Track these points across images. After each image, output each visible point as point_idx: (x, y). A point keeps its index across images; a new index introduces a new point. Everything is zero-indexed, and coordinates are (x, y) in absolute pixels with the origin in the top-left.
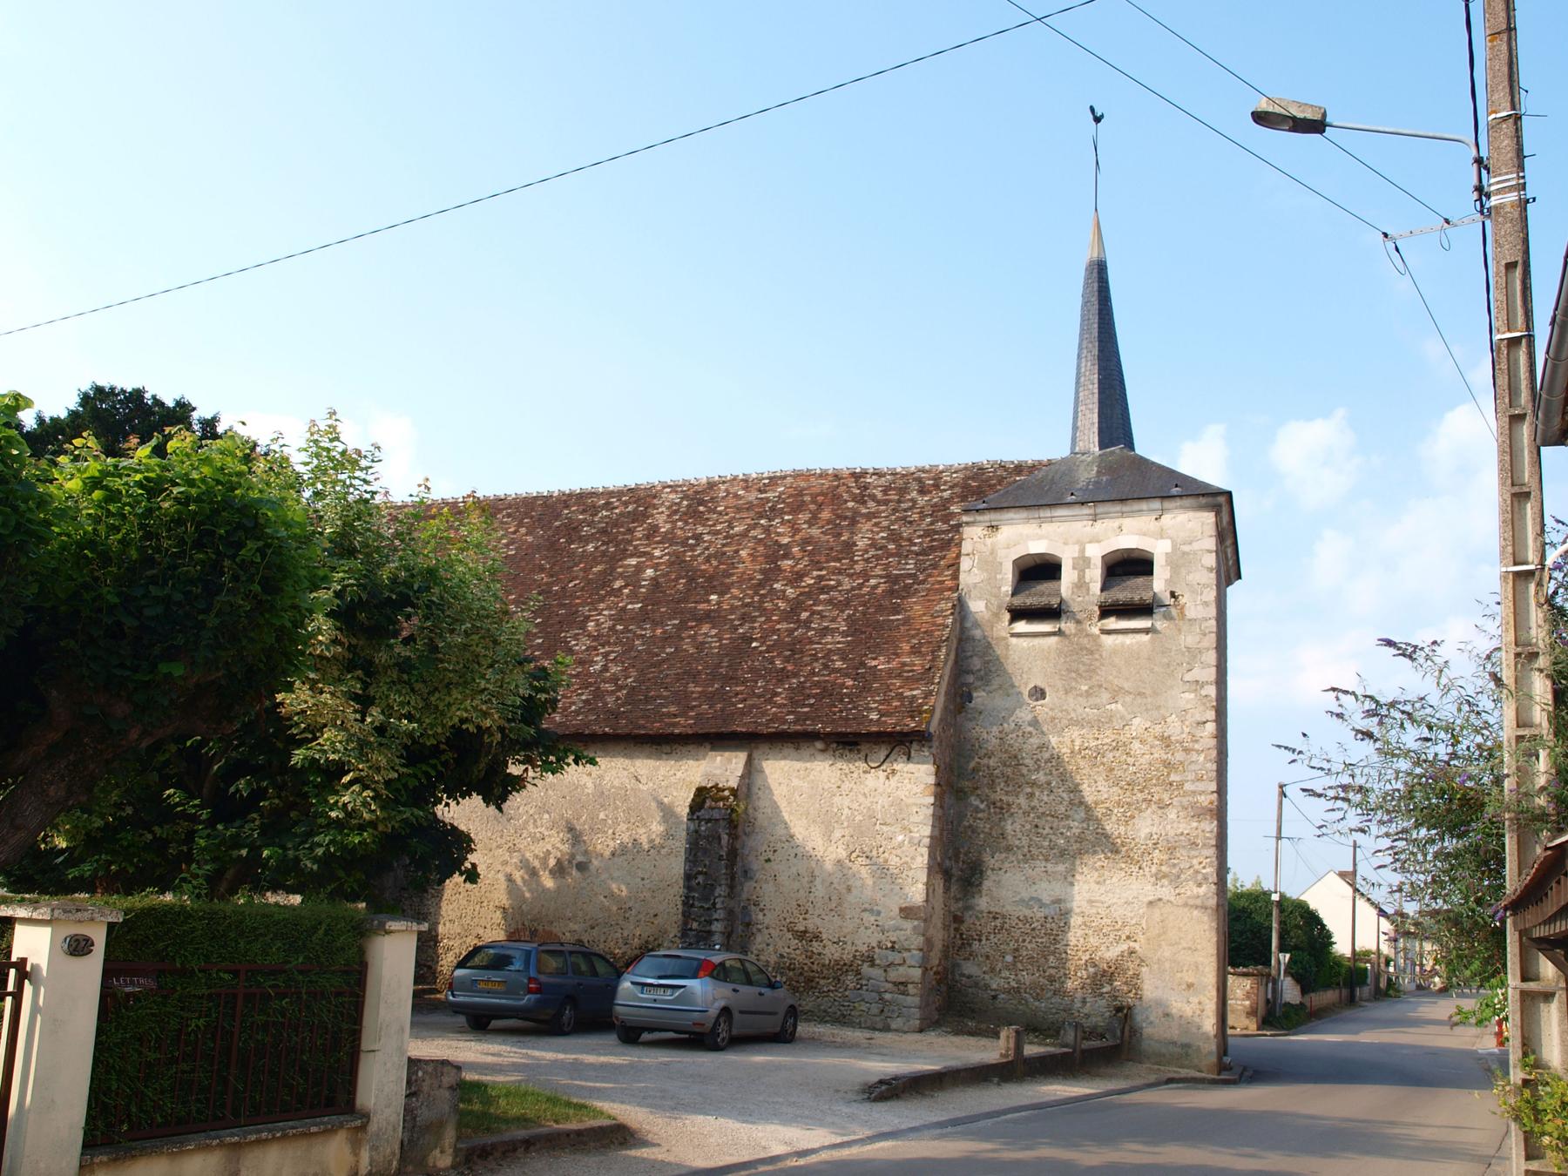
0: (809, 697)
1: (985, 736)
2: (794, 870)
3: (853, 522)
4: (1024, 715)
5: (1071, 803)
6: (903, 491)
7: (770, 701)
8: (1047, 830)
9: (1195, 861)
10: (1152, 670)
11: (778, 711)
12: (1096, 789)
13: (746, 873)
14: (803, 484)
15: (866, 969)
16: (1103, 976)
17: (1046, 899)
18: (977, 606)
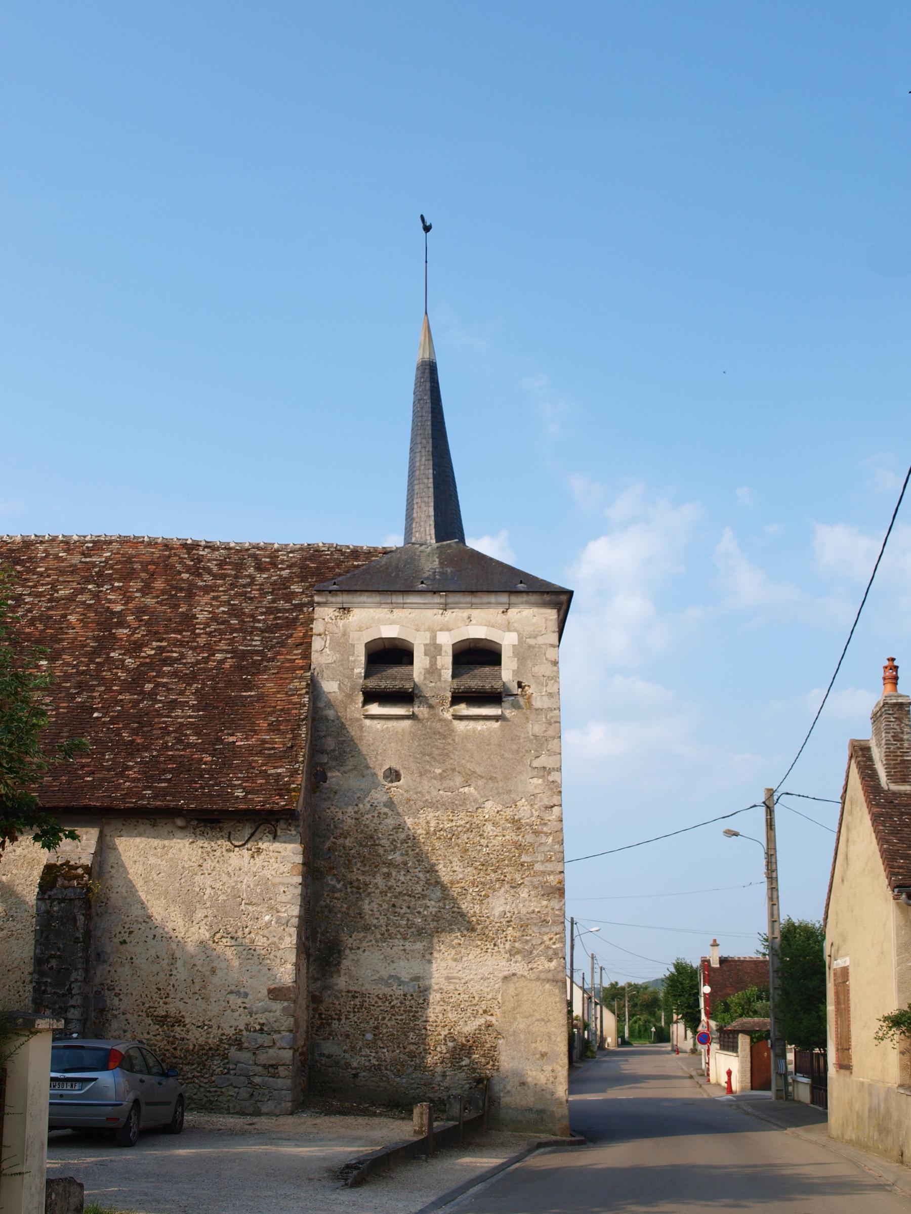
0: (165, 771)
1: (340, 816)
2: (152, 952)
3: (190, 595)
4: (378, 796)
5: (427, 882)
6: (239, 566)
7: (121, 775)
8: (405, 910)
9: (546, 938)
10: (502, 756)
11: (130, 783)
12: (452, 869)
13: (100, 957)
14: (130, 551)
15: (233, 1053)
16: (462, 1050)
17: (405, 977)
18: (330, 686)
